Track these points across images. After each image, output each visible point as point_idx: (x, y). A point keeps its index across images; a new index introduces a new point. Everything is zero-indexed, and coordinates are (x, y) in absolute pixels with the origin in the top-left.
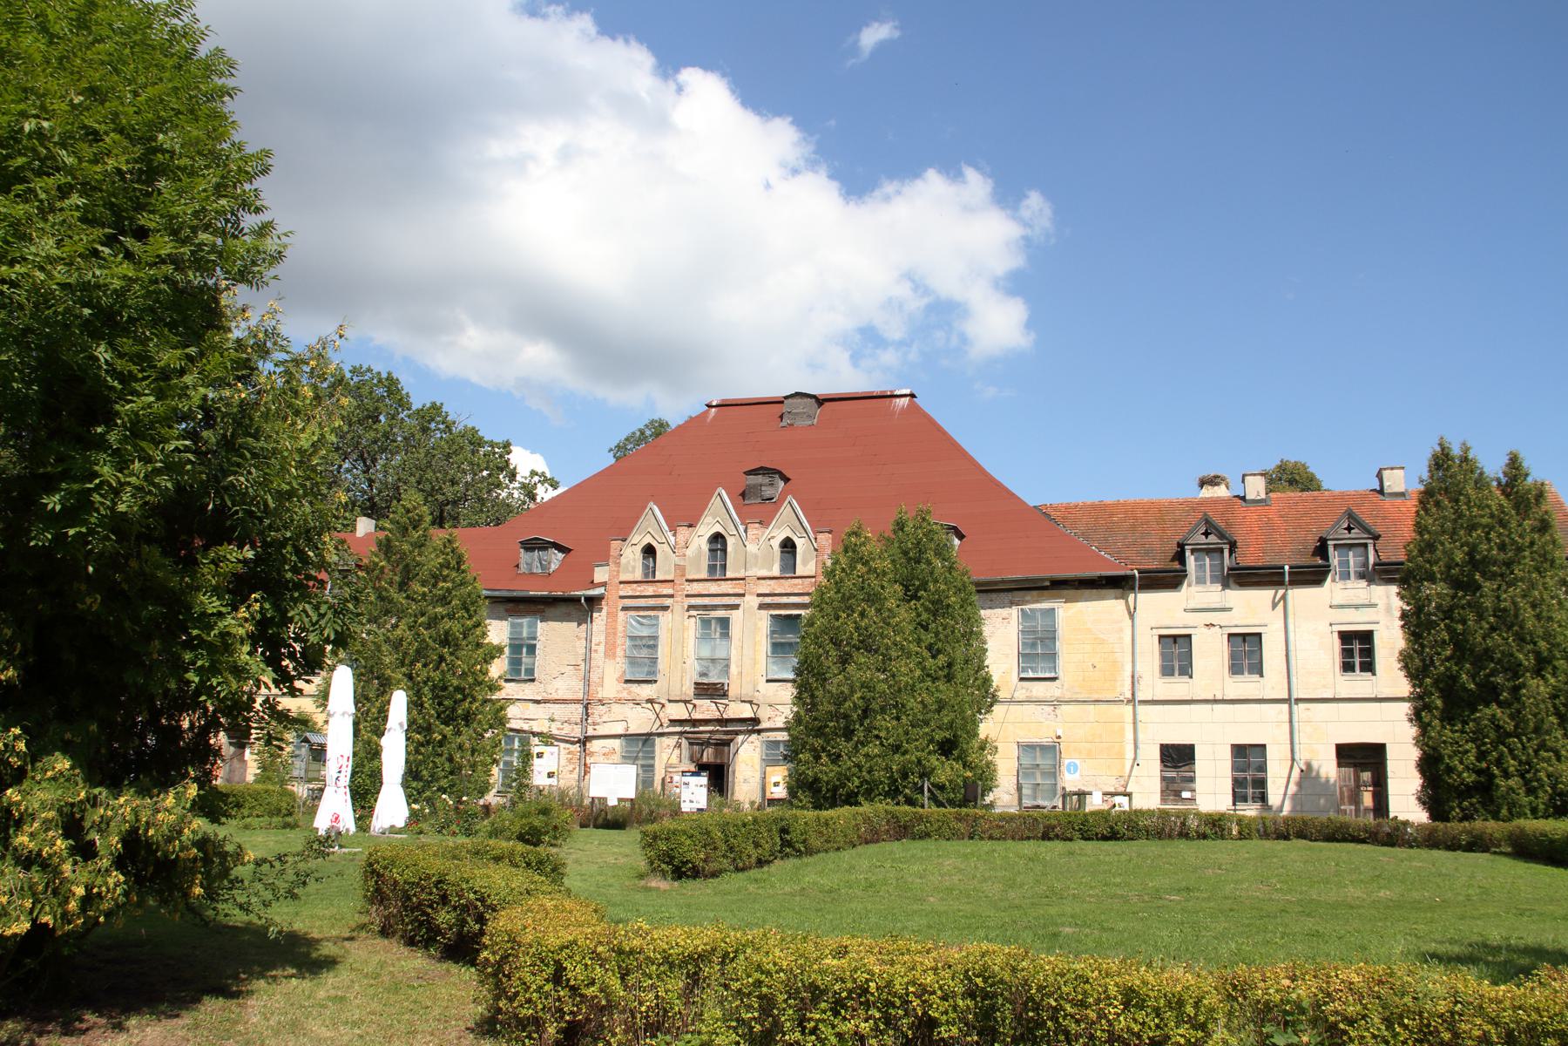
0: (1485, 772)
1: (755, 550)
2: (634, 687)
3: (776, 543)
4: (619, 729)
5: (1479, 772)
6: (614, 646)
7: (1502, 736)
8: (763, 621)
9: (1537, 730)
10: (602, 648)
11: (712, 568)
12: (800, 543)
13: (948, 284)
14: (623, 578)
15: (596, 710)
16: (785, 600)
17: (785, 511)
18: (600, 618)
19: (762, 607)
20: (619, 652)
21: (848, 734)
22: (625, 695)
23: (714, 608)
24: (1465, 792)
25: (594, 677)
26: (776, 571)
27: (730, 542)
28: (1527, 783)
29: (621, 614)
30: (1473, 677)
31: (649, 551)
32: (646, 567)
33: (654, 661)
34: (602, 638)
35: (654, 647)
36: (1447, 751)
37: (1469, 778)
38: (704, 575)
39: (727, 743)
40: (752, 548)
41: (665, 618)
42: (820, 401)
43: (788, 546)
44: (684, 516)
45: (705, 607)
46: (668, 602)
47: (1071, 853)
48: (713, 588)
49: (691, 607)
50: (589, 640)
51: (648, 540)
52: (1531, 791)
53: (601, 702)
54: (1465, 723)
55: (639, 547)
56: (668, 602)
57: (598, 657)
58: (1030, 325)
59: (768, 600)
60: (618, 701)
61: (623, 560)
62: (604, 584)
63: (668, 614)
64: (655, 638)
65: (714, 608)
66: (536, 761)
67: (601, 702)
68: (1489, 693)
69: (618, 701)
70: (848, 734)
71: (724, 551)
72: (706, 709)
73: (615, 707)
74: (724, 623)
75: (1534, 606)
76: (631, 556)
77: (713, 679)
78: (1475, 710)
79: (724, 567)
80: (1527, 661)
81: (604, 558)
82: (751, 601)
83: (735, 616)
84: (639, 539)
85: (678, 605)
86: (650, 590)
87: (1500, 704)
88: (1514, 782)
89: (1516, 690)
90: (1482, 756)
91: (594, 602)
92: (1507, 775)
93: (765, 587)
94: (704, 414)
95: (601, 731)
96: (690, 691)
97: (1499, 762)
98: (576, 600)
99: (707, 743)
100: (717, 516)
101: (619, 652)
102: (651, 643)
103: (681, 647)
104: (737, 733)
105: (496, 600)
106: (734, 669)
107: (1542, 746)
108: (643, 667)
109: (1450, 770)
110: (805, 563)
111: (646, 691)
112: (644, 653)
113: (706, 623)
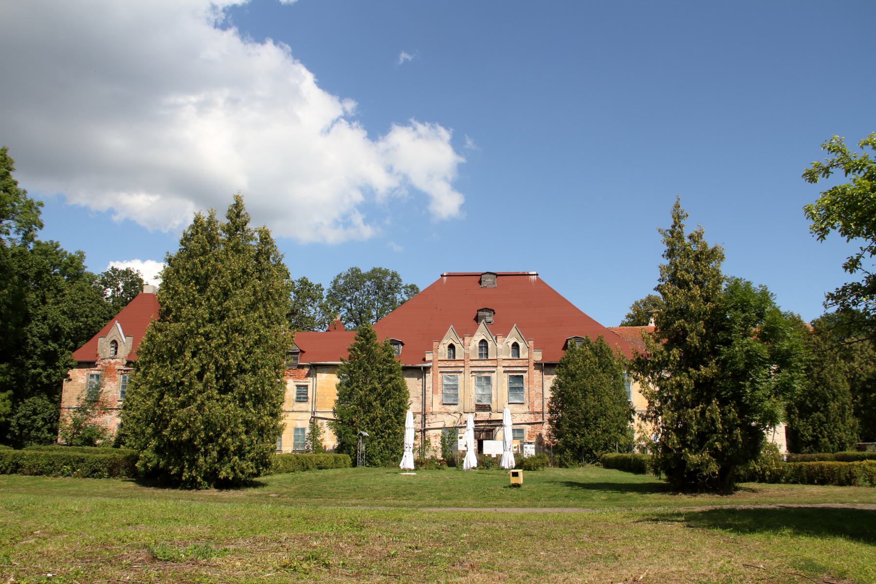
0: (816, 437)
1: (501, 347)
2: (447, 407)
3: (510, 345)
4: (441, 425)
5: (813, 436)
6: (437, 388)
7: (822, 423)
8: (506, 378)
9: (833, 421)
10: (431, 390)
11: (481, 355)
12: (521, 345)
13: (420, 182)
14: (440, 358)
15: (429, 418)
16: (515, 369)
17: (514, 330)
18: (429, 377)
19: (505, 372)
20: (440, 391)
21: (587, 426)
22: (443, 410)
23: (484, 372)
24: (808, 443)
25: (428, 402)
26: (510, 357)
27: (490, 344)
28: (830, 440)
29: (440, 375)
30: (811, 402)
31: (451, 347)
32: (449, 354)
33: (457, 395)
34: (431, 385)
35: (457, 389)
36: (801, 429)
37: (810, 438)
38: (478, 358)
39: (492, 431)
40: (499, 346)
41: (460, 377)
42: (497, 275)
43: (516, 346)
44: (464, 332)
45: (479, 372)
46: (462, 369)
47: (105, 506)
48: (483, 363)
49: (472, 372)
50: (424, 386)
51: (451, 342)
52: (832, 443)
53: (432, 413)
54: (807, 419)
55: (447, 346)
56: (462, 369)
57: (429, 394)
58: (462, 208)
59: (508, 369)
60: (440, 413)
61: (439, 351)
62: (430, 361)
63: (462, 375)
64: (457, 385)
65: (484, 372)
66: (459, 440)
67: (432, 413)
68: (816, 409)
69: (440, 413)
70: (587, 426)
71: (487, 347)
72: (484, 415)
73: (439, 416)
74: (488, 379)
75: (832, 376)
76: (443, 349)
77: (485, 402)
78: (811, 414)
79: (487, 354)
80: (830, 396)
81: (431, 349)
82: (501, 369)
83: (493, 376)
84: (447, 342)
85: (468, 370)
86: (453, 364)
87: (821, 412)
88: (826, 439)
89: (825, 407)
90: (814, 430)
91: (426, 369)
92: (823, 437)
93: (506, 363)
94: (439, 282)
95: (432, 426)
96: (474, 408)
97: (821, 432)
98: (420, 368)
99: (483, 431)
100: (481, 333)
101: (440, 391)
102: (455, 388)
103: (469, 389)
104: (496, 426)
105: (405, 369)
106: (494, 399)
107: (835, 427)
108: (451, 398)
109: (803, 436)
110: (523, 353)
111: (453, 408)
112: (452, 392)
113: (480, 378)
